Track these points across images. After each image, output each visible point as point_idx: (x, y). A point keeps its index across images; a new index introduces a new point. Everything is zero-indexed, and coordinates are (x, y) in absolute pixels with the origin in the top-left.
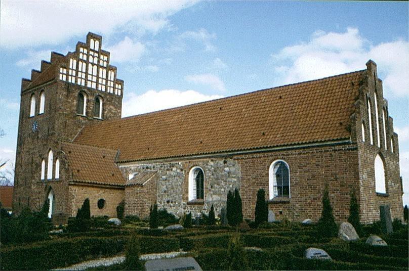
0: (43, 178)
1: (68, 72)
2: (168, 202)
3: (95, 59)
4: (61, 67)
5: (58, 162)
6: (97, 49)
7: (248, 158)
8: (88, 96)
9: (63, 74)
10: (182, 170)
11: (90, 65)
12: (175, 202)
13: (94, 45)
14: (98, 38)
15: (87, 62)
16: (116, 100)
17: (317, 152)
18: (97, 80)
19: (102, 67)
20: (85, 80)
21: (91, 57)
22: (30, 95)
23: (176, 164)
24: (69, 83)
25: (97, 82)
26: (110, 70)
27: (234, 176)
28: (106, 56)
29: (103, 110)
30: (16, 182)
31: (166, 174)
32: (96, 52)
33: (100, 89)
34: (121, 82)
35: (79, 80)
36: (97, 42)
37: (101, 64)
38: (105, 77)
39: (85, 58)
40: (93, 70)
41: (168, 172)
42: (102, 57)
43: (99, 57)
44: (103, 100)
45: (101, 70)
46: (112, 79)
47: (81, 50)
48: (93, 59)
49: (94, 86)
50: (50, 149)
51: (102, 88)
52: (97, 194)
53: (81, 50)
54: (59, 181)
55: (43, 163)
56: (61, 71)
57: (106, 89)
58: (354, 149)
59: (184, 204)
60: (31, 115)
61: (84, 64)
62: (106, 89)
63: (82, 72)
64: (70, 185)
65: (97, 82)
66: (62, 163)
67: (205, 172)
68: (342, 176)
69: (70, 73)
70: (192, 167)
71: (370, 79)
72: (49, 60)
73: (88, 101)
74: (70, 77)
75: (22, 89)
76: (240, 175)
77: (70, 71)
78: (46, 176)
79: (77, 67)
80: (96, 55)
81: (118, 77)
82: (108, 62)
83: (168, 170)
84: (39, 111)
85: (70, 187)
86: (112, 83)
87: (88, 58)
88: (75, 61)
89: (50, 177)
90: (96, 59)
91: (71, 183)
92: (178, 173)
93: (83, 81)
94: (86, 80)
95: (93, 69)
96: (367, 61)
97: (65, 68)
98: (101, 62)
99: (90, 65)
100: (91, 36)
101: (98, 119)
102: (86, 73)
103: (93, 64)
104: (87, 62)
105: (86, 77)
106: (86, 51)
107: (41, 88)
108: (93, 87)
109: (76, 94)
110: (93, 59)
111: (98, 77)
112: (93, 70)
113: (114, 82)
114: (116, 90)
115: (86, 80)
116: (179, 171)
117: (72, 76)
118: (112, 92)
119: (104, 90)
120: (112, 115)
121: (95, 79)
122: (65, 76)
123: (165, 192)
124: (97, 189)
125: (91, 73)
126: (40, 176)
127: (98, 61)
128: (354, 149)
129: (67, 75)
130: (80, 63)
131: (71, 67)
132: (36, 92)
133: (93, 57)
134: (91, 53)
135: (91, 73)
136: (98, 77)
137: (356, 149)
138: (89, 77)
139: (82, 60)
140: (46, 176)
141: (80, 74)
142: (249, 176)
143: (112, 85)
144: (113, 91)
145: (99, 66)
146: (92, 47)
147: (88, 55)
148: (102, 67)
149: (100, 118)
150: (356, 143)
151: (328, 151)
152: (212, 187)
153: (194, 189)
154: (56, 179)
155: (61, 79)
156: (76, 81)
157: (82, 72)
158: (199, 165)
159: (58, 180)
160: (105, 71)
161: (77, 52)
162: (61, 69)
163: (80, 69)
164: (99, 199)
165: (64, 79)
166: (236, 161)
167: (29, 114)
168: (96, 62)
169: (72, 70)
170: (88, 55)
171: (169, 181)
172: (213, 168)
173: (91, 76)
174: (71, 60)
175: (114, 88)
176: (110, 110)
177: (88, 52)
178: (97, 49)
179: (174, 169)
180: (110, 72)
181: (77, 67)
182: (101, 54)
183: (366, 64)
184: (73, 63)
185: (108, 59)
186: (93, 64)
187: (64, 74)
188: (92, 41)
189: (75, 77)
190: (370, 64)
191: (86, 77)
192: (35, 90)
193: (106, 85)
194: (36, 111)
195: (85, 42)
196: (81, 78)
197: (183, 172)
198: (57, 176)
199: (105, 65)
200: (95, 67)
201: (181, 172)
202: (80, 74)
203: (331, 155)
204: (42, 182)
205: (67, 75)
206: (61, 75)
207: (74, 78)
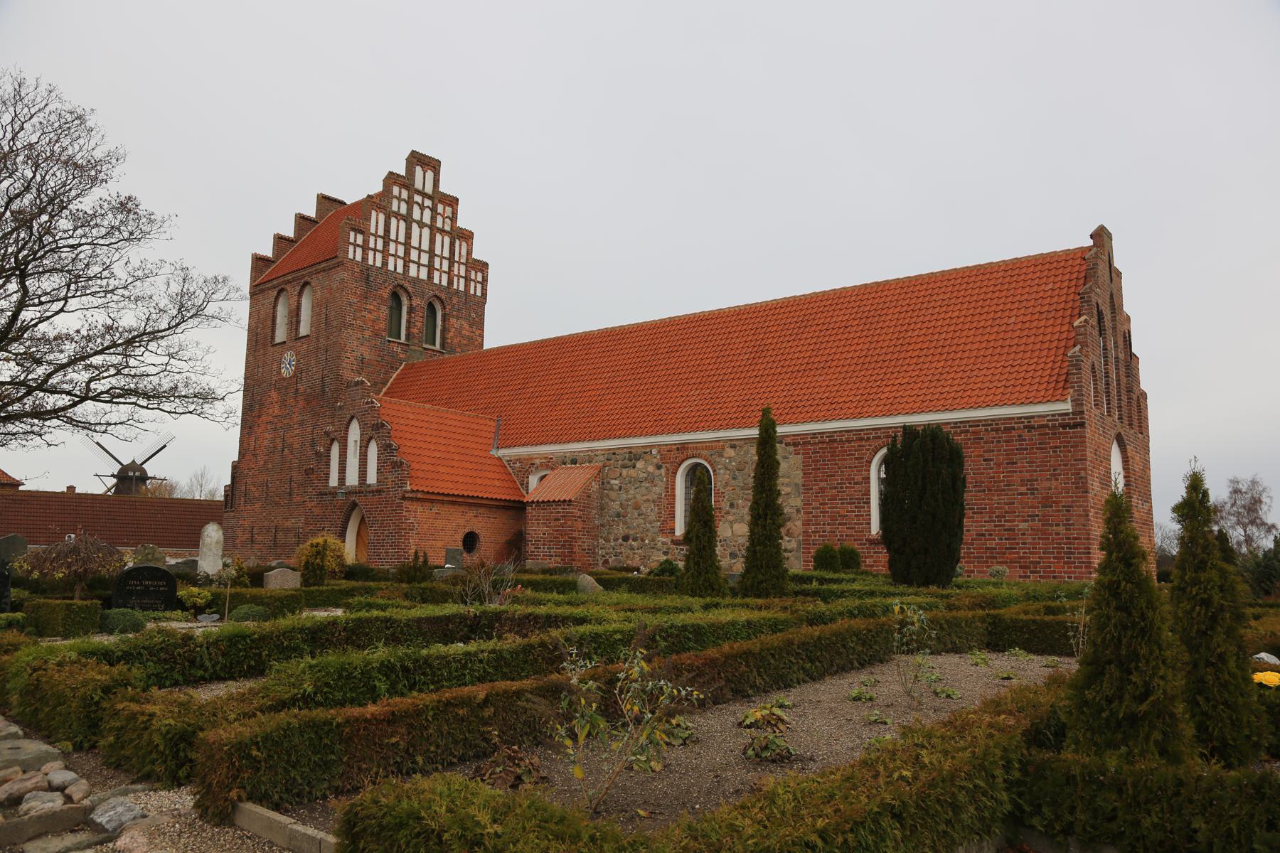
0: (334, 482)
1: (366, 242)
2: (626, 538)
3: (424, 212)
4: (353, 229)
5: (373, 450)
6: (429, 189)
7: (820, 442)
8: (410, 298)
9: (356, 245)
10: (659, 467)
11: (415, 227)
12: (643, 540)
13: (422, 179)
14: (432, 165)
15: (408, 219)
16: (474, 308)
17: (987, 430)
18: (429, 262)
19: (442, 231)
20: (405, 262)
21: (416, 208)
22: (298, 288)
23: (645, 453)
24: (369, 268)
25: (431, 267)
26: (460, 238)
27: (787, 480)
28: (449, 205)
29: (444, 331)
30: (231, 491)
31: (621, 475)
32: (429, 197)
33: (436, 281)
34: (482, 267)
35: (391, 260)
36: (430, 175)
37: (439, 224)
38: (446, 254)
39: (403, 210)
40: (420, 237)
41: (625, 472)
42: (440, 208)
43: (433, 210)
44: (444, 308)
45: (438, 237)
46: (463, 260)
47: (396, 190)
48: (422, 214)
49: (423, 274)
50: (352, 418)
51: (440, 279)
52: (462, 522)
53: (396, 190)
54: (377, 491)
55: (335, 451)
56: (352, 240)
57: (450, 282)
58: (1075, 426)
59: (664, 543)
60: (278, 339)
61: (402, 224)
62: (450, 282)
63: (396, 241)
64: (404, 498)
65: (431, 267)
66: (386, 449)
67: (714, 471)
68: (1047, 484)
69: (372, 245)
70: (683, 461)
71: (1102, 270)
72: (311, 213)
73: (411, 310)
74: (371, 254)
75: (253, 279)
76: (800, 480)
77: (372, 239)
78: (342, 479)
79: (387, 230)
80: (428, 203)
81: (475, 255)
82: (454, 218)
83: (624, 467)
84: (297, 329)
85: (406, 504)
86: (463, 268)
87: (410, 210)
88: (382, 217)
89: (352, 479)
90: (427, 213)
91: (407, 496)
92: (649, 473)
93: (400, 263)
94: (407, 261)
95: (421, 236)
96: (1093, 228)
97: (362, 232)
98: (439, 219)
99: (415, 226)
100: (417, 159)
101: (433, 351)
102: (407, 245)
103: (421, 225)
104: (408, 219)
105: (407, 253)
106: (405, 194)
107: (304, 276)
108: (420, 277)
109: (386, 293)
110: (422, 214)
111: (431, 253)
112: (420, 237)
113: (466, 265)
114: (472, 284)
115: (407, 261)
116: (651, 469)
117: (375, 250)
118: (462, 288)
119: (444, 283)
120: (465, 342)
121: (425, 259)
122: (359, 251)
123: (618, 515)
124: (461, 509)
125: (417, 246)
126: (327, 479)
127: (433, 219)
128: (1075, 426)
129: (365, 248)
130: (394, 221)
131: (373, 230)
132: (288, 287)
133: (422, 208)
134: (418, 198)
135: (417, 246)
136: (431, 253)
137: (1082, 425)
138: (414, 255)
139: (397, 215)
140: (342, 479)
141: (392, 245)
142: (821, 480)
143: (463, 273)
144: (466, 286)
145: (433, 228)
146: (418, 185)
147: (410, 203)
148: (442, 231)
149: (438, 346)
150: (1082, 412)
151: (1013, 428)
152: (732, 506)
153: (1254, 483)
154: (369, 486)
155: (351, 256)
156: (385, 263)
157: (396, 241)
158: (699, 456)
159: (374, 489)
160: (447, 240)
161: (386, 193)
162: (352, 234)
163: (393, 236)
164: (467, 531)
165: (359, 258)
166: (791, 449)
167: (273, 337)
168: (427, 219)
169: (376, 236)
170: (410, 203)
171: (627, 491)
172: (734, 464)
173: (417, 252)
174: (374, 213)
175: (467, 279)
176: (459, 331)
177: (410, 197)
178: (429, 189)
179: (640, 465)
180: (457, 242)
181: (387, 230)
182: (440, 202)
183: (1092, 236)
184: (377, 221)
185: (453, 213)
186: (421, 225)
187: (358, 245)
188: (419, 170)
189: (382, 252)
190: (1101, 236)
191: (407, 253)
192: (289, 282)
193: (449, 272)
194: (290, 329)
195: (403, 173)
196: (395, 256)
197: (663, 471)
198: (372, 478)
199: (447, 228)
200: (426, 232)
201: (657, 472)
202: (392, 246)
203: (1021, 438)
204: (333, 493)
205: (365, 248)
206: (351, 248)
207: (379, 256)
